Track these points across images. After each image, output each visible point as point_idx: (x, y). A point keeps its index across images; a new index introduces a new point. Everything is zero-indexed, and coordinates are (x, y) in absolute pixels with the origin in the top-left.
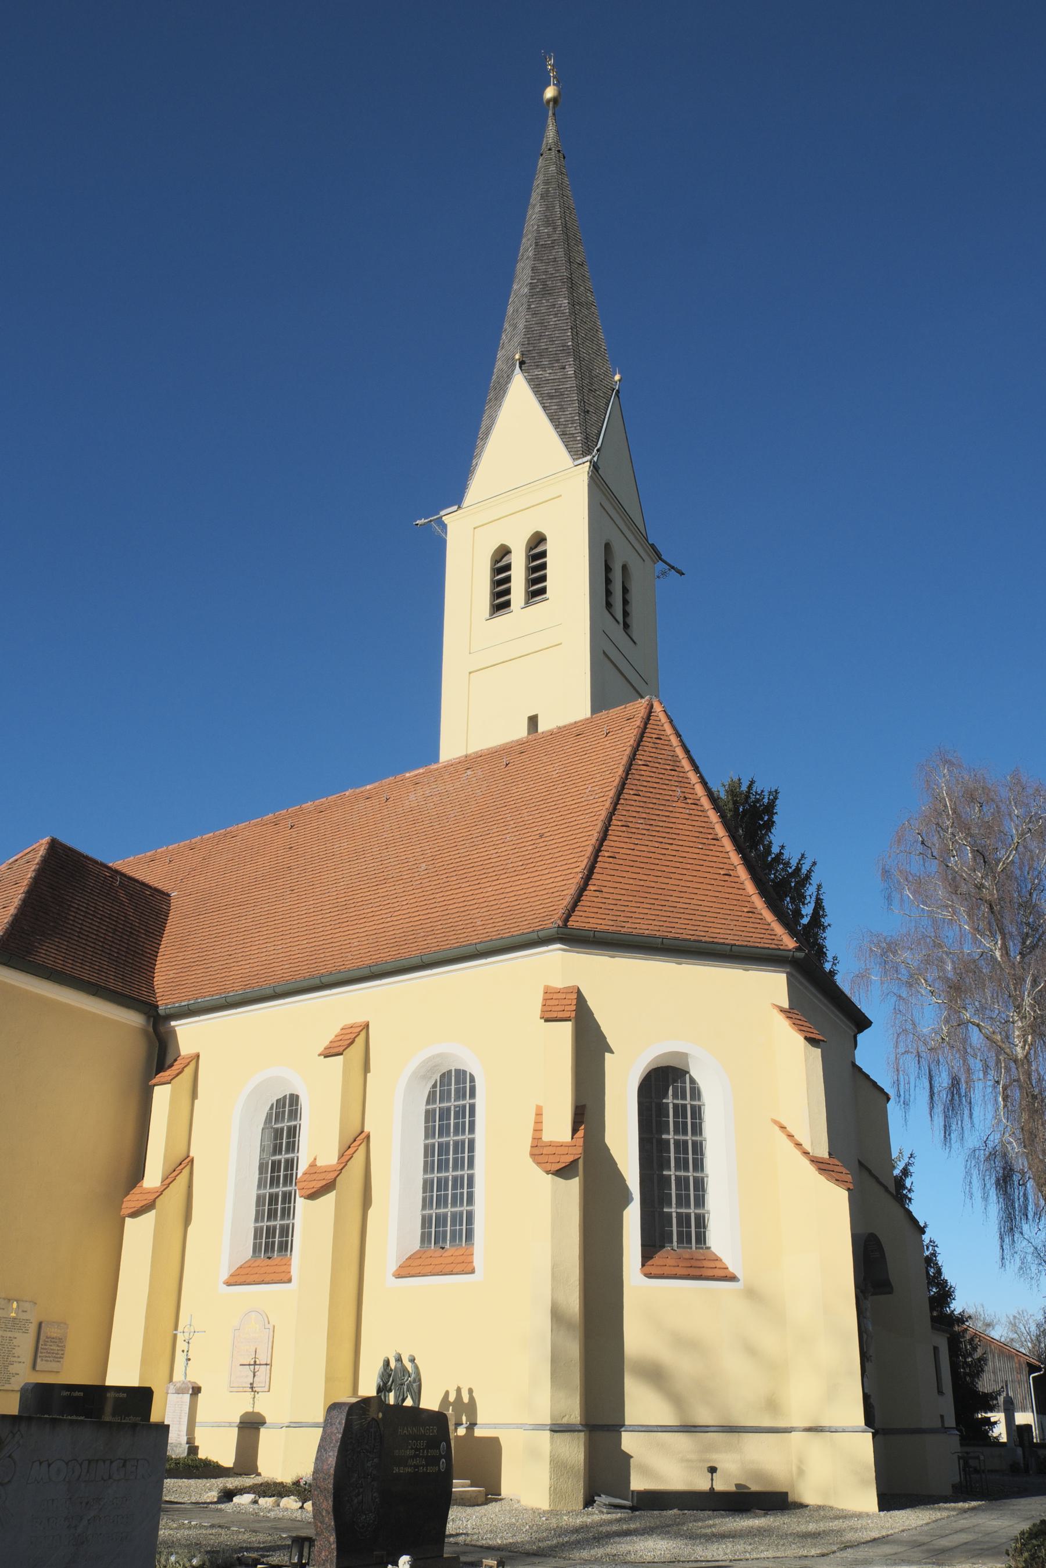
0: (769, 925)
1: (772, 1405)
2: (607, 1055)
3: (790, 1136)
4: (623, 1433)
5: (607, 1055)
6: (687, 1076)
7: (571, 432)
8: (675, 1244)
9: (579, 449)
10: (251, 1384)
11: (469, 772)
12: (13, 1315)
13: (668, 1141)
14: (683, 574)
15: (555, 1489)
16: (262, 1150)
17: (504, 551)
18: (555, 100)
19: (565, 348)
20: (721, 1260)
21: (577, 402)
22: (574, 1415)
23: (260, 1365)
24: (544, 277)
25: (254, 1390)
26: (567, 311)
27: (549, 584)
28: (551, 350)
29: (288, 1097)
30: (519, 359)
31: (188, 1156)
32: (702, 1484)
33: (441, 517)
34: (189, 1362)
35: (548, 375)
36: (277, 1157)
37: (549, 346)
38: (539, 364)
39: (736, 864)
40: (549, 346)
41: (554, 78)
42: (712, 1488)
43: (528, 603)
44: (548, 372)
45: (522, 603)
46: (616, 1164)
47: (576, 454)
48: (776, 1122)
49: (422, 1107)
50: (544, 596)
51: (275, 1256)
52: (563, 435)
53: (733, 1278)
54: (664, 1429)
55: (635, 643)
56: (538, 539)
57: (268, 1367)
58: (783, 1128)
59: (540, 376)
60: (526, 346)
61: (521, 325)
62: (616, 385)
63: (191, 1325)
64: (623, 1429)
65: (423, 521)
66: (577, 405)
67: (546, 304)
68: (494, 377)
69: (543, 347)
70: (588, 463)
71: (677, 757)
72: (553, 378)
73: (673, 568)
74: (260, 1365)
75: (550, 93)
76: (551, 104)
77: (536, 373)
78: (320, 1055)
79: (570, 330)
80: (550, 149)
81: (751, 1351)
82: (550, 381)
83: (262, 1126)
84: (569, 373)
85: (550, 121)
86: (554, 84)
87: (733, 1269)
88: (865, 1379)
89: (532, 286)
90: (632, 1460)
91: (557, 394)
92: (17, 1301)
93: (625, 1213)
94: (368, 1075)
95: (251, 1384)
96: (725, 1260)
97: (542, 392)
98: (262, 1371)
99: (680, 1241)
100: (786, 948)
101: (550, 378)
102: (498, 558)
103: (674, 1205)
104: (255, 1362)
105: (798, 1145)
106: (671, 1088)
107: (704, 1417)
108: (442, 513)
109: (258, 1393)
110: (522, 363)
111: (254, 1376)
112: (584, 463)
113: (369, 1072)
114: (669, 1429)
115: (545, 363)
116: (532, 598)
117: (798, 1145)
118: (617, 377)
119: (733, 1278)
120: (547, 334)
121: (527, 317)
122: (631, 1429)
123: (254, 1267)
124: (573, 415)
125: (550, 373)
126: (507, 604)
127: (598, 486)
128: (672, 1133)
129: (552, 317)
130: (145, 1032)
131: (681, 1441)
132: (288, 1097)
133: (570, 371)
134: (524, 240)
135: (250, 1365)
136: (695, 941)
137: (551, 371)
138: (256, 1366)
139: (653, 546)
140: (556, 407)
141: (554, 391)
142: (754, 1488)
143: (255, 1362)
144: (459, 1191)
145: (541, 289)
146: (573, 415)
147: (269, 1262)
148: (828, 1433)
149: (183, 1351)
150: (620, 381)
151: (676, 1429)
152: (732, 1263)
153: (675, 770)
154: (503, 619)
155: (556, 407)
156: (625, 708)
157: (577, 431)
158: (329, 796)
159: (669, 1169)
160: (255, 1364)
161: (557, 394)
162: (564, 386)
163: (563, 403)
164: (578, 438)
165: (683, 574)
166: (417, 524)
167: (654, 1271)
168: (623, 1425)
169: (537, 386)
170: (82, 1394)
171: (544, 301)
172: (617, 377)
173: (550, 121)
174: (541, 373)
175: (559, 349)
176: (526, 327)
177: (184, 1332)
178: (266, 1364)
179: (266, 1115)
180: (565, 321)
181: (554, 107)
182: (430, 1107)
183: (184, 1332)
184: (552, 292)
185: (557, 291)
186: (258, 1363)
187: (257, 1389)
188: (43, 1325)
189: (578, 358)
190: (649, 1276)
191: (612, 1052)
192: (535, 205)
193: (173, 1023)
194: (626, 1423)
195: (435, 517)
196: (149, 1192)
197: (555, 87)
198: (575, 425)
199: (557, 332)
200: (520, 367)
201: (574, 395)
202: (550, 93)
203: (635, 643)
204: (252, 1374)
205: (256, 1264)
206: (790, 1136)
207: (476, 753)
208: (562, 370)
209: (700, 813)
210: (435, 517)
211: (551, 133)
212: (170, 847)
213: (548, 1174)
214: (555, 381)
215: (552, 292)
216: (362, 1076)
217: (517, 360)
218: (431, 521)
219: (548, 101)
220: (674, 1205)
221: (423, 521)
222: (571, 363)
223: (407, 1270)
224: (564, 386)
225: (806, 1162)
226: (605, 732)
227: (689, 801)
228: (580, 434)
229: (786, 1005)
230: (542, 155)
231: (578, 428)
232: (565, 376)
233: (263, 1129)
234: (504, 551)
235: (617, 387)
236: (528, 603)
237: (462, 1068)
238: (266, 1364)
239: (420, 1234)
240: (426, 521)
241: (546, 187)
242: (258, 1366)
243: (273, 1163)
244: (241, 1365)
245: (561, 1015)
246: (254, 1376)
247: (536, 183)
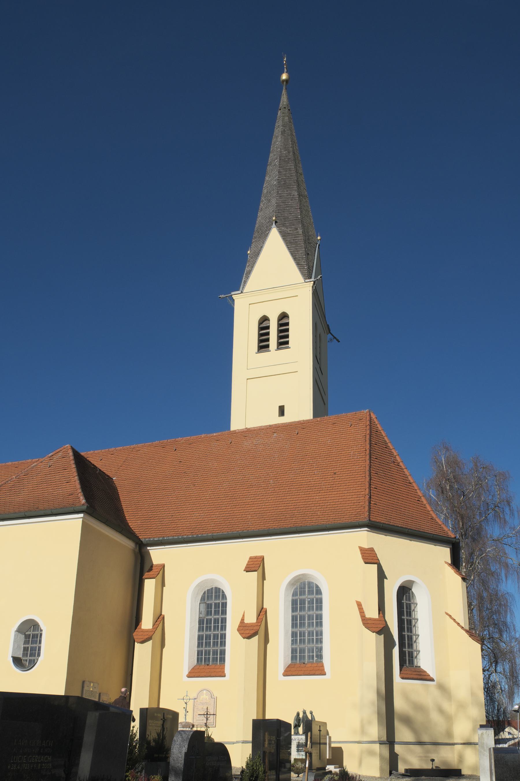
0: (440, 525)
1: (449, 734)
2: (385, 580)
3: (454, 620)
4: (395, 745)
5: (385, 580)
6: (411, 591)
7: (302, 264)
8: (407, 665)
9: (306, 273)
10: (205, 723)
11: (275, 435)
12: (91, 689)
13: (404, 619)
14: (339, 342)
15: (381, 768)
16: (200, 613)
17: (264, 319)
18: (287, 81)
19: (297, 218)
20: (426, 672)
21: (304, 248)
22: (384, 738)
23: (210, 715)
24: (285, 177)
25: (207, 726)
26: (297, 198)
27: (291, 339)
28: (290, 218)
29: (214, 588)
30: (275, 220)
31: (161, 615)
32: (428, 766)
33: (232, 296)
34: (187, 713)
35: (289, 231)
36: (209, 617)
37: (289, 216)
38: (284, 224)
39: (421, 496)
40: (289, 216)
41: (286, 68)
42: (432, 768)
43: (278, 349)
44: (289, 229)
45: (276, 348)
46: (390, 629)
47: (307, 275)
48: (447, 614)
49: (290, 598)
50: (287, 346)
51: (211, 664)
52: (298, 264)
53: (432, 680)
54: (405, 743)
55: (322, 374)
56: (284, 316)
57: (215, 716)
58: (450, 616)
59: (285, 231)
60: (277, 213)
61: (274, 201)
62: (318, 242)
63: (187, 696)
64: (395, 743)
65: (223, 296)
66: (304, 250)
67: (286, 193)
68: (257, 226)
69: (286, 216)
70: (313, 282)
71: (386, 441)
72: (291, 233)
73: (335, 338)
74: (210, 715)
75: (284, 76)
76: (285, 83)
77: (283, 229)
78: (244, 571)
79: (299, 210)
80: (285, 108)
81: (441, 711)
82: (290, 235)
83: (199, 602)
84: (300, 232)
85: (284, 92)
86: (286, 72)
87: (432, 675)
88: (128, 701)
89: (279, 182)
90: (399, 756)
91: (294, 242)
92: (93, 683)
93: (393, 650)
94: (265, 581)
95: (205, 723)
96: (428, 672)
97: (286, 240)
98: (211, 718)
99: (409, 663)
100: (450, 537)
101: (290, 233)
102: (261, 322)
103: (407, 648)
104: (207, 713)
105: (458, 624)
106: (405, 596)
107: (426, 738)
108: (233, 293)
109: (209, 728)
110: (276, 222)
111: (207, 720)
112: (310, 282)
113: (265, 580)
114: (411, 743)
115: (287, 224)
116: (280, 345)
117: (458, 624)
118: (319, 238)
119: (432, 680)
120: (287, 209)
121: (277, 198)
122: (398, 743)
123: (201, 669)
124: (302, 255)
125: (290, 230)
126: (268, 346)
127: (315, 296)
128: (405, 616)
129: (290, 200)
130: (134, 551)
131: (417, 749)
132: (214, 588)
133: (300, 231)
134: (271, 155)
135: (204, 715)
136: (401, 527)
137: (290, 229)
138: (208, 715)
139: (328, 325)
140: (294, 249)
141: (292, 240)
142: (442, 767)
143: (207, 713)
144: (311, 638)
145: (283, 184)
146: (302, 255)
147: (207, 667)
148: (474, 745)
149: (184, 708)
150: (320, 240)
151: (414, 743)
152: (431, 672)
153: (387, 448)
154: (264, 355)
155: (294, 249)
156: (356, 413)
157: (305, 264)
158: (192, 436)
159: (405, 632)
160: (207, 714)
161: (294, 242)
162: (297, 239)
163: (297, 248)
164: (306, 268)
165: (339, 342)
166: (220, 297)
167: (405, 676)
168: (395, 742)
169: (284, 236)
170: (266, 733)
171: (285, 191)
172: (319, 238)
173: (284, 92)
174: (286, 229)
175: (294, 218)
176: (276, 203)
177: (183, 699)
178: (214, 715)
179: (201, 596)
180: (296, 204)
181: (286, 85)
182: (294, 598)
183: (183, 699)
184: (289, 186)
185: (291, 186)
186: (209, 713)
187: (209, 726)
188: (101, 694)
189: (303, 225)
190: (403, 678)
191: (387, 579)
192: (278, 137)
193: (148, 548)
194: (396, 741)
195: (229, 295)
196: (147, 631)
197: (286, 74)
198: (304, 260)
199: (292, 209)
200: (275, 224)
201: (303, 244)
202: (284, 76)
203: (322, 374)
204: (206, 719)
205: (200, 668)
206: (454, 620)
207: (276, 425)
208: (296, 230)
209: (401, 470)
210: (229, 295)
211: (284, 99)
212: (96, 452)
213: (373, 632)
214: (292, 235)
215: (289, 186)
216: (262, 582)
217: (274, 220)
218: (227, 297)
219: (283, 81)
220: (407, 648)
221: (223, 296)
222: (300, 227)
223: (289, 672)
224: (297, 239)
225: (464, 632)
226: (350, 424)
227: (396, 464)
228: (306, 266)
229: (450, 562)
230: (280, 110)
231: (305, 262)
232: (297, 233)
233: (200, 604)
234: (264, 319)
235: (319, 242)
236: (278, 349)
237: (312, 581)
238: (214, 715)
239: (291, 656)
240: (224, 296)
241: (284, 128)
242: (209, 716)
243: (207, 620)
244: (199, 715)
245: (373, 561)
246: (207, 720)
247: (277, 124)
